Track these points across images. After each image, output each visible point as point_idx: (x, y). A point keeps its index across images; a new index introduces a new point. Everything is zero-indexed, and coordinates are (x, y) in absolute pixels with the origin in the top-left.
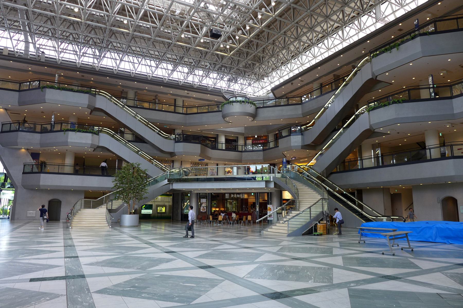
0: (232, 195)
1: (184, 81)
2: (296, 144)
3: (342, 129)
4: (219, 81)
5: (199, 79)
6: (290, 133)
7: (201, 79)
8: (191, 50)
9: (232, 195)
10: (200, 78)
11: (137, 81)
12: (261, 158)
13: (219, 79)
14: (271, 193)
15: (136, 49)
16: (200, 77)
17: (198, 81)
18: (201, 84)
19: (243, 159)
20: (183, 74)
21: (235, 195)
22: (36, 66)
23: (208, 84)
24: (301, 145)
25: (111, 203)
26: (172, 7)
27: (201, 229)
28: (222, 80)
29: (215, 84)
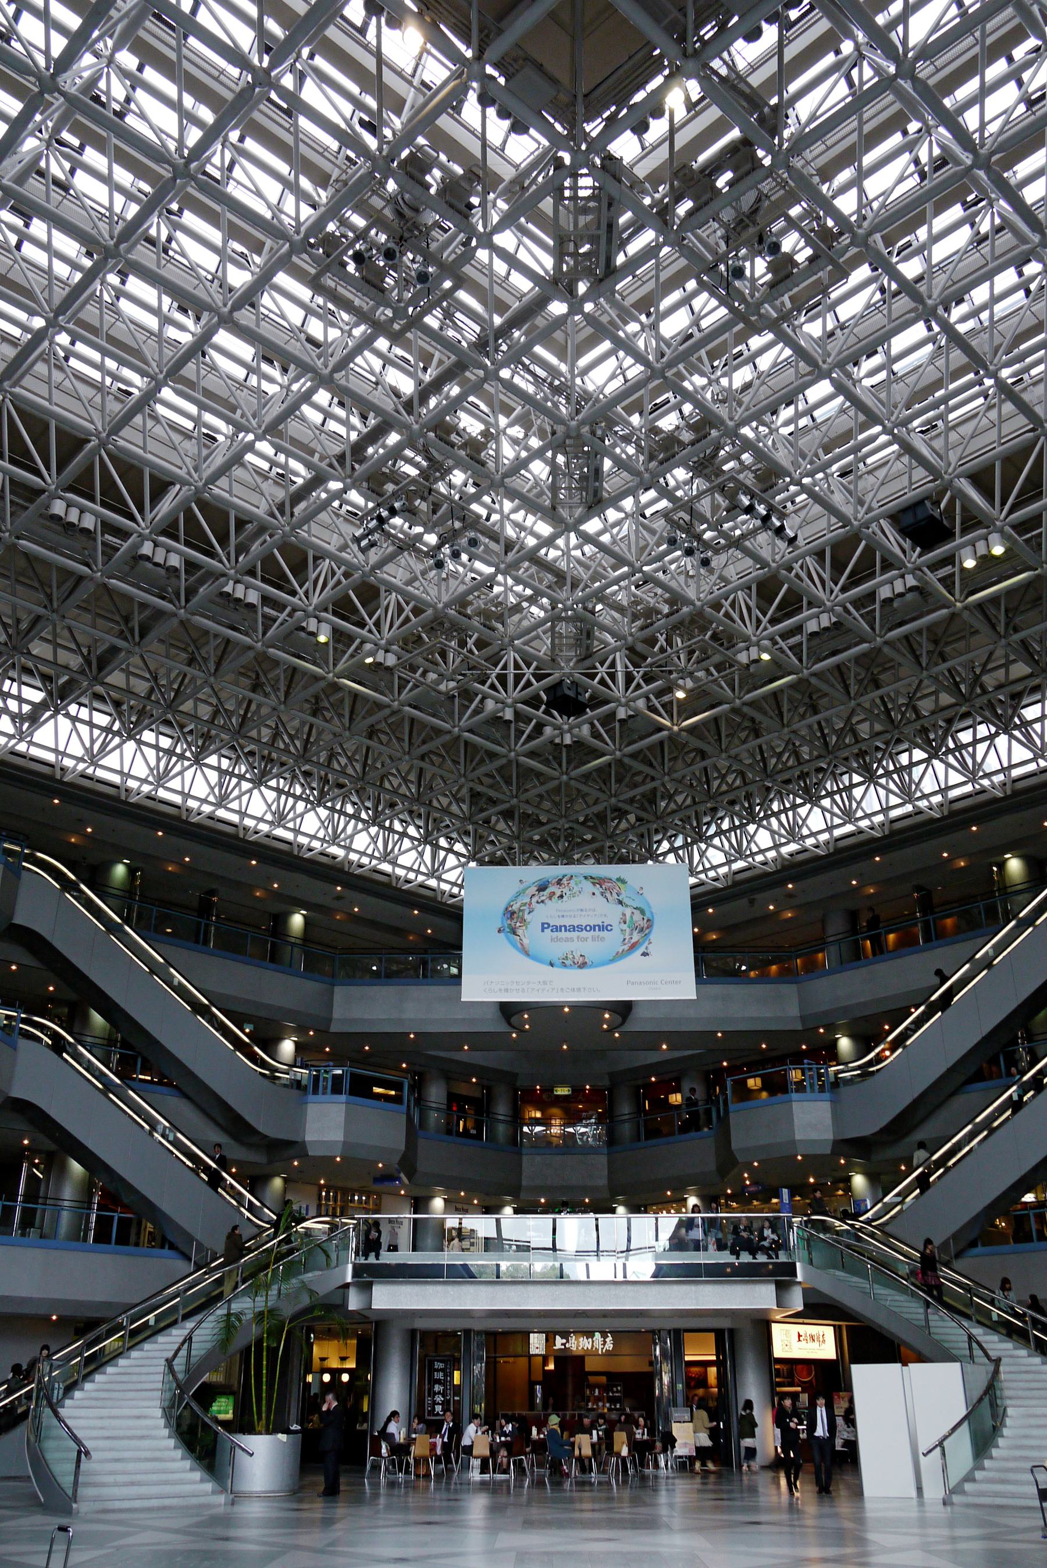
0: (559, 1341)
1: (13, 742)
2: (814, 1136)
3: (1014, 1088)
4: (117, 740)
5: (88, 745)
6: (777, 1086)
7: (96, 747)
8: (161, 630)
9: (559, 1341)
10: (93, 741)
11: (168, 829)
12: (601, 1180)
13: (118, 733)
14: (732, 1331)
15: (128, 680)
16: (96, 732)
17: (147, 771)
18: (90, 771)
19: (524, 1183)
20: (84, 729)
21: (573, 1339)
22: (381, 902)
23: (128, 775)
24: (832, 1137)
25: (180, 1376)
26: (126, 432)
27: (14, 1518)
28: (130, 737)
29: (92, 756)
